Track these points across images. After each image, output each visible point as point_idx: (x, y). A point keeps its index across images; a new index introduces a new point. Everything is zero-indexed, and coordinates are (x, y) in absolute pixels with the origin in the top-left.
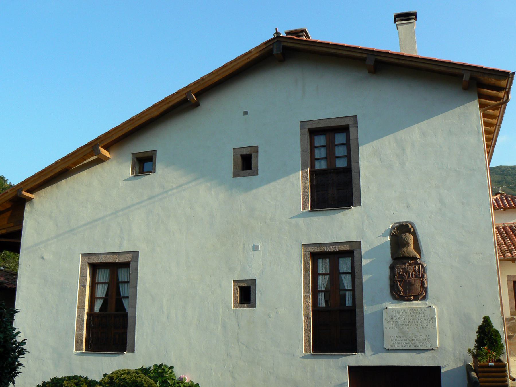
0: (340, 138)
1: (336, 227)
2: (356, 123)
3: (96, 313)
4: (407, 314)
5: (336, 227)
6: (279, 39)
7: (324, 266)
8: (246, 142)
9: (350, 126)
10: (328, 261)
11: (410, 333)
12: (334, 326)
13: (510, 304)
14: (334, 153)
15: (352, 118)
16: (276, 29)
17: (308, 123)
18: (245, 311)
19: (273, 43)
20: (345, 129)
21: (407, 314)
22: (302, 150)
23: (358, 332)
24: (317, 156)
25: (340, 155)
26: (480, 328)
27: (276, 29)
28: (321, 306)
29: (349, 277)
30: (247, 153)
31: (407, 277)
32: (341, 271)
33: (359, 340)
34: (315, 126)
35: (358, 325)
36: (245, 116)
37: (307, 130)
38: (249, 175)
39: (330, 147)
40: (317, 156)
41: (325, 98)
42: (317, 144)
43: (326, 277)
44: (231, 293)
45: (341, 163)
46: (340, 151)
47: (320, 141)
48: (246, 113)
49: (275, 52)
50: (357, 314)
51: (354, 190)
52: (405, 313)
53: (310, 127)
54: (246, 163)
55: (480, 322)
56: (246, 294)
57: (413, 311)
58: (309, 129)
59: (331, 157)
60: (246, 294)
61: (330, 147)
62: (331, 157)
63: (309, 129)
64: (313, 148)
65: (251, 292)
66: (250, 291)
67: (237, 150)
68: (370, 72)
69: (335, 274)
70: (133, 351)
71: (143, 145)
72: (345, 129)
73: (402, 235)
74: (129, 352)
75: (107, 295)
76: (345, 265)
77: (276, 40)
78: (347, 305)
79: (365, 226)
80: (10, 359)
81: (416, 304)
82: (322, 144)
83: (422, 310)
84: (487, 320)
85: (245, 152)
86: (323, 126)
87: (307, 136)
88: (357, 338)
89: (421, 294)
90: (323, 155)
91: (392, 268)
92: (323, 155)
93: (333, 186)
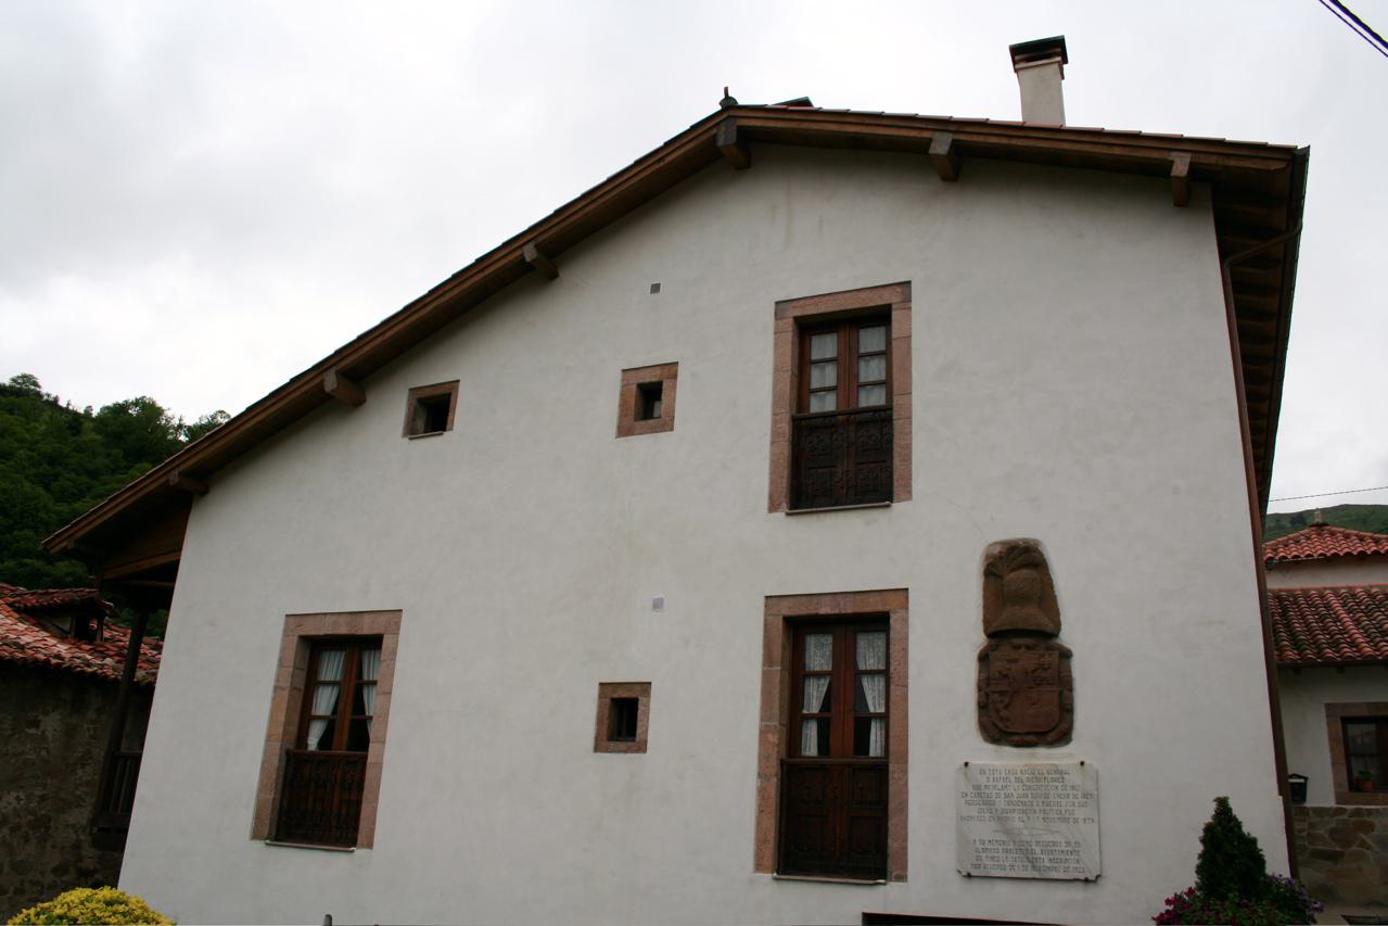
0: (870, 340)
1: (838, 555)
2: (907, 299)
3: (312, 752)
4: (1018, 780)
5: (838, 555)
6: (732, 113)
7: (819, 654)
8: (647, 356)
9: (894, 307)
10: (830, 639)
11: (1025, 832)
12: (830, 808)
13: (1336, 773)
14: (857, 376)
15: (899, 289)
16: (726, 90)
17: (795, 304)
18: (619, 763)
19: (718, 124)
20: (880, 317)
21: (1018, 780)
22: (777, 370)
23: (893, 822)
24: (815, 384)
25: (871, 379)
26: (1208, 829)
27: (726, 90)
28: (808, 754)
29: (880, 682)
30: (654, 380)
31: (1027, 687)
32: (862, 667)
33: (893, 844)
34: (811, 310)
35: (892, 805)
36: (654, 295)
37: (791, 320)
38: (654, 430)
39: (848, 361)
40: (815, 384)
41: (827, 243)
42: (816, 355)
43: (822, 681)
44: (586, 715)
45: (872, 399)
46: (872, 371)
47: (825, 346)
48: (656, 288)
49: (721, 142)
50: (890, 776)
51: (896, 461)
52: (1012, 778)
53: (798, 313)
54: (648, 401)
55: (1207, 814)
56: (622, 718)
57: (1036, 776)
58: (796, 319)
59: (849, 382)
60: (622, 718)
61: (848, 361)
62: (849, 382)
63: (796, 319)
64: (887, 384)
65: (639, 712)
66: (636, 709)
67: (629, 373)
68: (945, 179)
69: (846, 676)
70: (370, 845)
71: (431, 374)
72: (880, 317)
73: (1018, 583)
74: (363, 846)
75: (335, 711)
76: (868, 654)
77: (725, 115)
78: (872, 754)
79: (918, 556)
80: (1288, 894)
81: (1043, 757)
82: (828, 356)
83: (1060, 774)
84: (1223, 806)
85: (649, 378)
86: (830, 310)
87: (789, 336)
88: (890, 841)
89: (1055, 728)
90: (831, 381)
91: (983, 658)
92: (831, 381)
93: (840, 453)
